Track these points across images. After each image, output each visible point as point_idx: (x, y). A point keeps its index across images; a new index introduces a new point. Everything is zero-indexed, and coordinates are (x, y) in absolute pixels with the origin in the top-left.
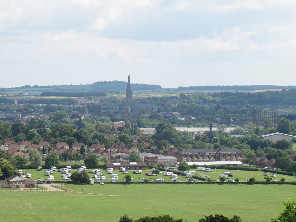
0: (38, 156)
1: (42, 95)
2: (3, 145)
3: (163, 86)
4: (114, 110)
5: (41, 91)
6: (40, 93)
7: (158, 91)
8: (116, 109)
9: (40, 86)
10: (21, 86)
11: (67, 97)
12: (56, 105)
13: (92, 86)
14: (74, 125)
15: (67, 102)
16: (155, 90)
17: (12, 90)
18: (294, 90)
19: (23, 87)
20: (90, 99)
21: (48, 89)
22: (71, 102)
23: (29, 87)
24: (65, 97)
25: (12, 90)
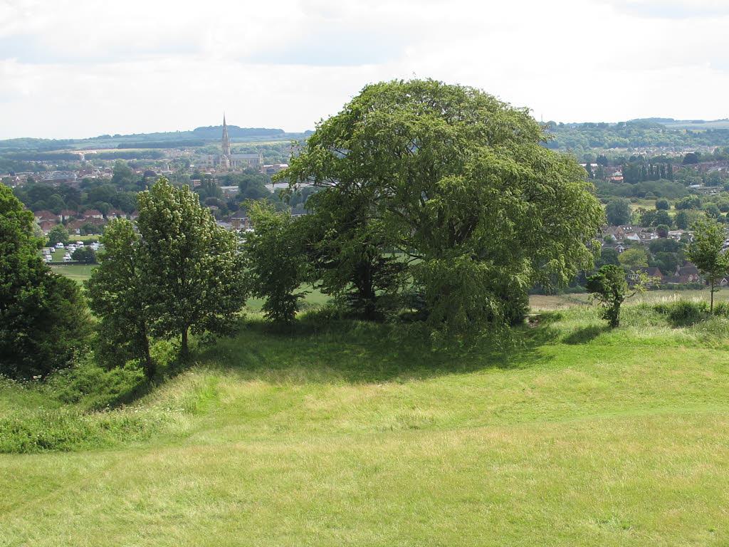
0: (38, 230)
1: (120, 147)
2: (622, 300)
3: (287, 131)
4: (207, 164)
5: (118, 142)
6: (117, 145)
7: (279, 137)
8: (210, 163)
9: (122, 135)
10: (97, 136)
11: (152, 149)
12: (135, 160)
13: (192, 133)
14: (137, 186)
15: (150, 156)
16: (276, 136)
17: (85, 142)
18: (724, 131)
19: (99, 138)
20: (182, 150)
21: (135, 139)
22: (156, 156)
23: (107, 137)
24: (147, 149)
25: (85, 142)
